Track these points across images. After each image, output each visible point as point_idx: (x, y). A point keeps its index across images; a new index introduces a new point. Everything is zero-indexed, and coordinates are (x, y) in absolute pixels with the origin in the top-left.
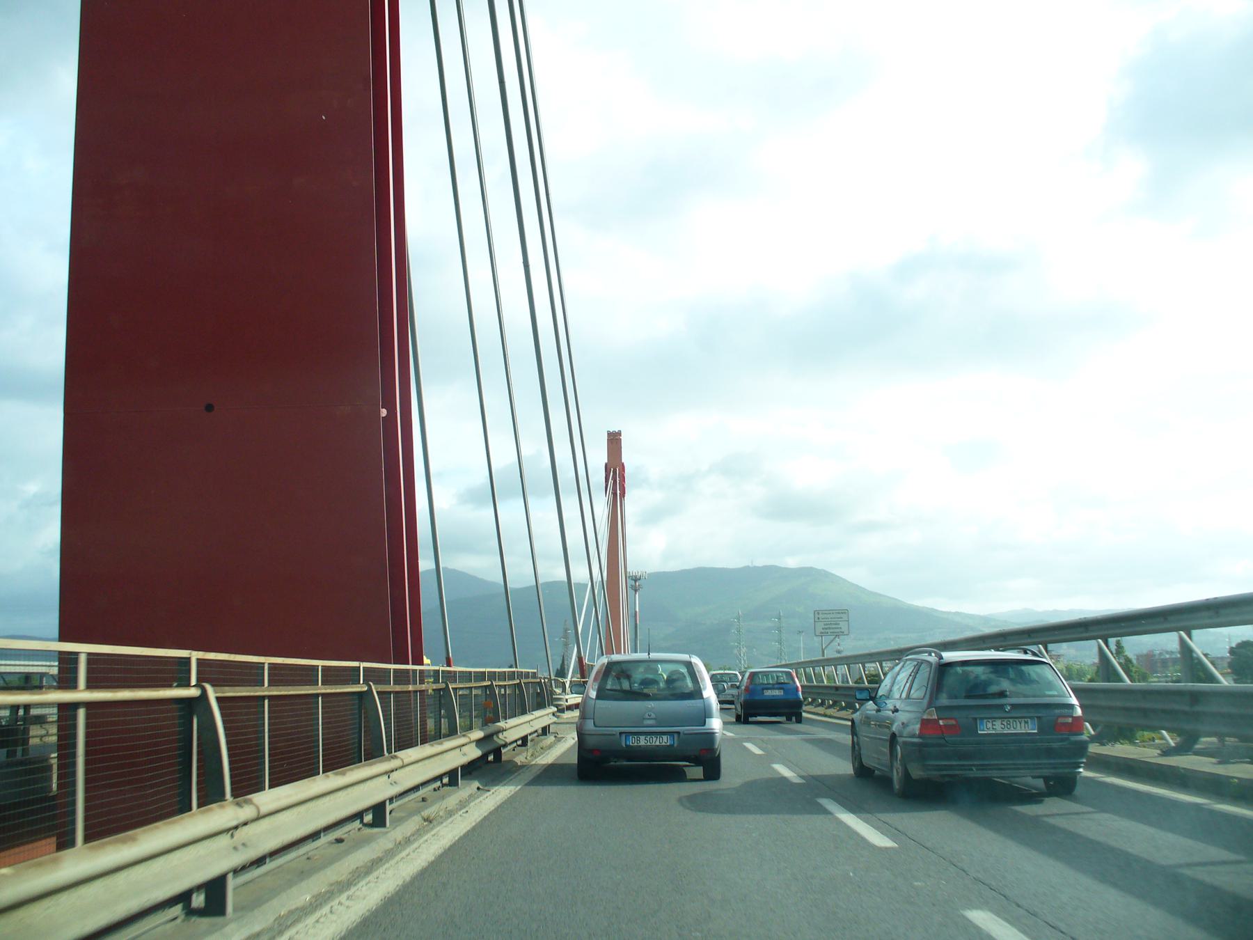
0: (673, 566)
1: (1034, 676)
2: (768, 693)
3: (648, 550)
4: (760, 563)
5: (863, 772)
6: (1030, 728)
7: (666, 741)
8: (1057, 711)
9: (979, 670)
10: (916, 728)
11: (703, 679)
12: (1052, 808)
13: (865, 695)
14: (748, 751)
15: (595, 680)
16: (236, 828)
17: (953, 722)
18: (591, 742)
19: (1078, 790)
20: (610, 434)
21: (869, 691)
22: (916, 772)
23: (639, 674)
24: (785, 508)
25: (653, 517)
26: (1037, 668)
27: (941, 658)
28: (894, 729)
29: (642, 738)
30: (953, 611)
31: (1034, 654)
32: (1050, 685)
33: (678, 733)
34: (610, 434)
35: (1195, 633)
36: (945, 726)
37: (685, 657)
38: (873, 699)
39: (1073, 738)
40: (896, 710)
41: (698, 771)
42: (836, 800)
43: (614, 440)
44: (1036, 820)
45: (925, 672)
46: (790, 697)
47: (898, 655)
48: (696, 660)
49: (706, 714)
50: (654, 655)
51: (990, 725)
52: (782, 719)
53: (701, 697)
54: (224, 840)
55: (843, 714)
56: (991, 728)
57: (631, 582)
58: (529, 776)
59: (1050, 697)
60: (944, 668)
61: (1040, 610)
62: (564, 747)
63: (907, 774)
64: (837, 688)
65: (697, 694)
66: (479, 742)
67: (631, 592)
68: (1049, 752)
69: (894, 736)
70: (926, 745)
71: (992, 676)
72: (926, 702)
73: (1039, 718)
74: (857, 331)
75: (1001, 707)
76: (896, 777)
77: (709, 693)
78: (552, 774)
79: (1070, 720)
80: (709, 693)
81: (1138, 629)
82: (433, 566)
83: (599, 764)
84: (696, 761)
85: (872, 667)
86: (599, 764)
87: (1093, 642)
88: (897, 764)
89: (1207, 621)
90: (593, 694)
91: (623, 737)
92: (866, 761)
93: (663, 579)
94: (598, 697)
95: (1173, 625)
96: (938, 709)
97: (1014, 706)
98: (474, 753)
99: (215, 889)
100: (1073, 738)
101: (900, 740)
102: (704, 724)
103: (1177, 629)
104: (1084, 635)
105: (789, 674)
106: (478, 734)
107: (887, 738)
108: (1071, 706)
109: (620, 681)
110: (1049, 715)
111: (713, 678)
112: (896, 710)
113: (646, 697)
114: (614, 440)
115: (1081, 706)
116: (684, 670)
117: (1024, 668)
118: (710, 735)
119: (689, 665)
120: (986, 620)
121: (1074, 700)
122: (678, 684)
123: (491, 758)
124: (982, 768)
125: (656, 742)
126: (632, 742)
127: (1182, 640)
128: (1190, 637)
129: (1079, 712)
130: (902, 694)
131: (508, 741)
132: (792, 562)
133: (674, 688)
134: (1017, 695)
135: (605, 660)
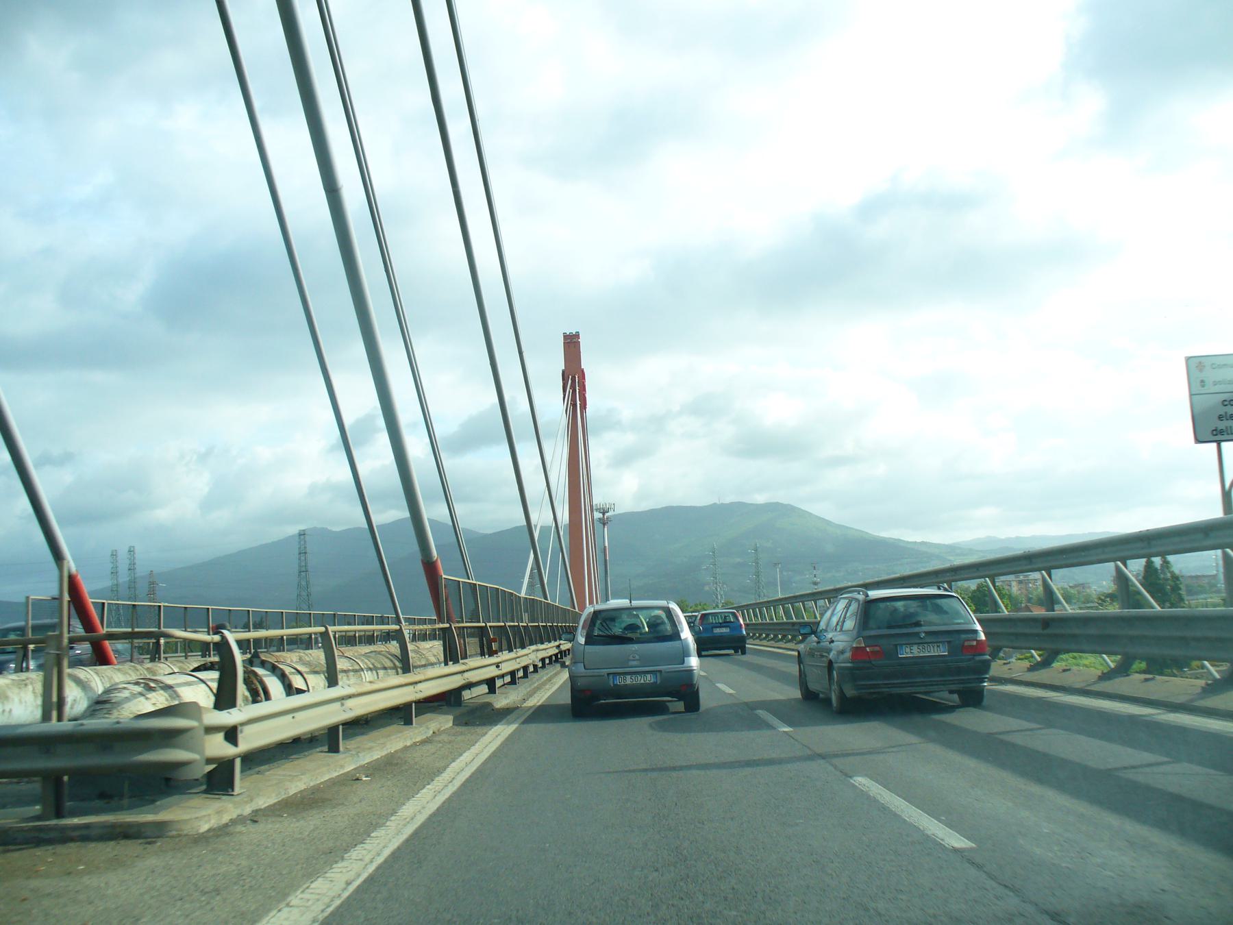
0: (644, 506)
2: (717, 631)
3: (619, 487)
4: (728, 499)
5: (809, 696)
6: (942, 651)
7: (649, 679)
8: (963, 636)
10: (848, 655)
11: (680, 623)
12: (969, 719)
13: (807, 630)
14: (719, 681)
17: (877, 649)
18: (580, 683)
19: (985, 702)
20: (566, 337)
22: (850, 692)
23: (627, 620)
24: (757, 445)
25: (624, 459)
28: (831, 656)
30: (919, 540)
31: (945, 590)
32: (957, 614)
34: (566, 337)
35: (1129, 562)
37: (663, 603)
38: (814, 632)
39: (978, 658)
40: (832, 641)
43: (572, 343)
45: (854, 607)
46: (736, 633)
47: (832, 595)
48: (673, 606)
49: (685, 653)
50: (636, 603)
53: (679, 638)
55: (789, 645)
56: (908, 652)
57: (597, 515)
60: (870, 603)
62: (554, 686)
65: (676, 636)
67: (598, 526)
68: (959, 671)
69: (830, 663)
70: (858, 669)
71: (919, 610)
72: (855, 632)
73: (949, 642)
74: (822, 271)
75: (917, 634)
77: (686, 634)
80: (686, 634)
82: (407, 514)
83: (590, 703)
86: (590, 703)
87: (1112, 564)
88: (835, 687)
90: (582, 640)
92: (813, 686)
93: (632, 519)
94: (586, 643)
97: (928, 633)
100: (978, 658)
101: (835, 665)
103: (1114, 560)
107: (826, 665)
108: (976, 632)
109: (608, 630)
110: (958, 638)
111: (248, 640)
112: (832, 641)
113: (629, 641)
114: (572, 343)
116: (663, 615)
117: (939, 601)
118: (690, 672)
119: (668, 612)
120: (952, 549)
121: (978, 627)
122: (661, 628)
124: (926, 693)
125: (641, 680)
126: (619, 681)
127: (1117, 568)
128: (1125, 565)
129: (982, 637)
130: (839, 625)
132: (760, 499)
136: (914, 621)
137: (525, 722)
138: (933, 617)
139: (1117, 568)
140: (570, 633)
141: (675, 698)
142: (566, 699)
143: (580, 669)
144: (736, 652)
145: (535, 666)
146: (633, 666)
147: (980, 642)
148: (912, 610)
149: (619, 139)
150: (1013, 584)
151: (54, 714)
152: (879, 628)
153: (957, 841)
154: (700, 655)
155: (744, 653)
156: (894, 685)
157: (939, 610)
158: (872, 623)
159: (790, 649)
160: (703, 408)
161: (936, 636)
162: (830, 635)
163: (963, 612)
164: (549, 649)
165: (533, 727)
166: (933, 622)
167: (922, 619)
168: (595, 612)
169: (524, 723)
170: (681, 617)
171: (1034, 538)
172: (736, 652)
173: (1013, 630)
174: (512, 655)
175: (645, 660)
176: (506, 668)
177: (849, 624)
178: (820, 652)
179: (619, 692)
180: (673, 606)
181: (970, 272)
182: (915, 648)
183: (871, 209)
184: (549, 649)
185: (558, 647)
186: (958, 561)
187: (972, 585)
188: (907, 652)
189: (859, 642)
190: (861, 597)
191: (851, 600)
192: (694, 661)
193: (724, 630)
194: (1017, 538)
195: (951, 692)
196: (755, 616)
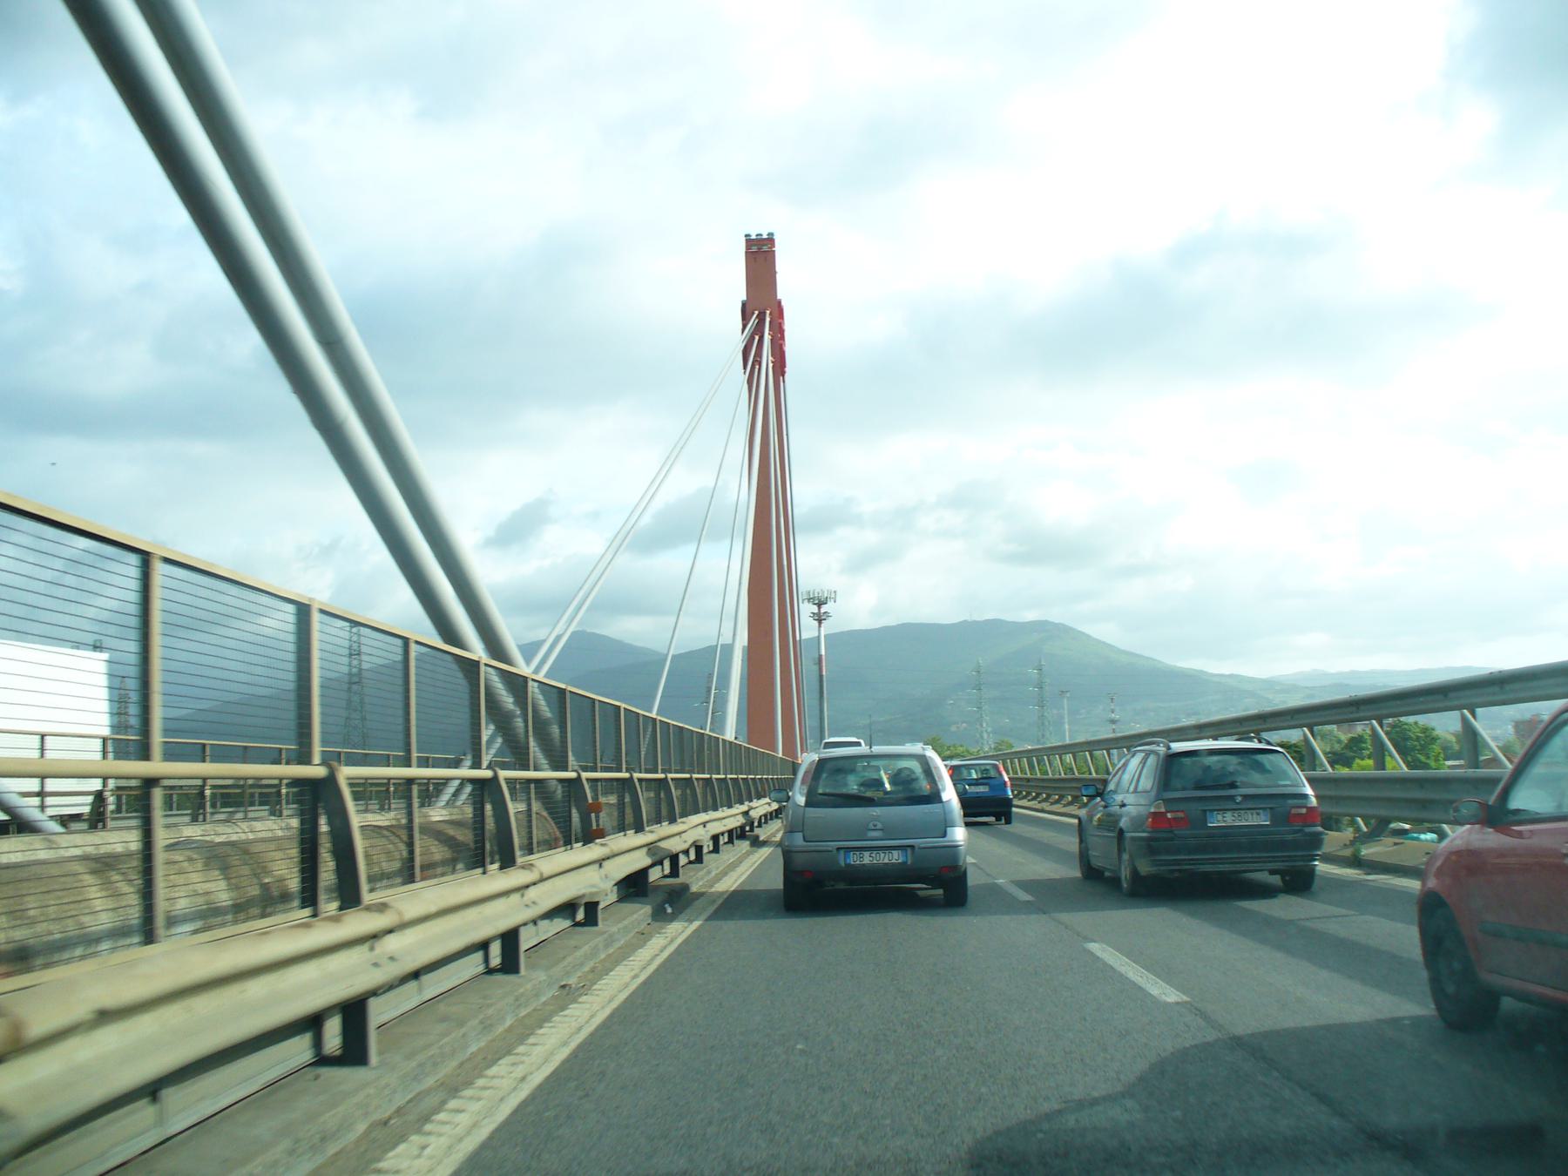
1: (1268, 766)
5: (1092, 873)
6: (1261, 820)
7: (896, 857)
9: (1233, 760)
11: (941, 777)
12: (1284, 907)
15: (803, 782)
16: (527, 887)
17: (1181, 815)
18: (800, 861)
19: (1316, 884)
20: (750, 242)
21: (1099, 789)
22: (1145, 868)
26: (1270, 757)
27: (1169, 748)
29: (866, 854)
32: (1284, 774)
33: (912, 847)
35: (1479, 711)
36: (1174, 819)
37: (916, 748)
38: (1100, 794)
39: (1307, 830)
40: (1123, 805)
43: (760, 253)
44: (1269, 922)
45: (1152, 760)
47: (1129, 742)
48: (931, 753)
49: (945, 825)
50: (877, 749)
52: (992, 819)
54: (515, 897)
56: (1221, 820)
59: (1284, 786)
63: (1135, 873)
64: (1028, 780)
65: (934, 797)
68: (1283, 845)
69: (1121, 832)
72: (1153, 793)
74: (1124, 327)
75: (1232, 798)
76: (1125, 873)
77: (949, 794)
78: (738, 904)
79: (1304, 811)
80: (949, 794)
81: (1522, 695)
84: (934, 880)
86: (813, 889)
87: (1456, 714)
89: (1491, 698)
95: (1456, 703)
96: (1167, 801)
97: (1246, 797)
100: (1307, 830)
101: (1128, 835)
102: (944, 835)
103: (1459, 708)
104: (1441, 705)
105: (996, 767)
108: (1305, 796)
109: (837, 785)
110: (1281, 803)
112: (1123, 805)
114: (760, 253)
115: (1317, 797)
117: (1260, 757)
119: (922, 759)
120: (1270, 684)
121: (1309, 791)
122: (915, 785)
125: (884, 858)
126: (854, 859)
128: (1474, 716)
129: (1314, 801)
130: (1133, 784)
133: (913, 790)
134: (1245, 785)
135: (816, 757)
136: (1229, 780)
137: (715, 916)
138: (1256, 777)
139: (1464, 719)
140: (782, 789)
141: (939, 886)
142: (775, 881)
143: (798, 840)
144: (998, 819)
145: (699, 849)
147: (1311, 809)
148: (1231, 768)
152: (1184, 789)
153: (1171, 996)
154: (967, 824)
155: (1008, 822)
156: (1222, 861)
157: (1260, 768)
158: (1176, 783)
159: (1068, 815)
161: (1256, 801)
162: (1119, 798)
163: (1291, 772)
164: (730, 818)
165: (729, 926)
166: (1256, 783)
167: (1239, 779)
169: (709, 919)
170: (941, 768)
171: (1373, 672)
172: (998, 819)
173: (1332, 793)
174: (515, 878)
175: (888, 832)
176: (690, 837)
177: (1146, 783)
178: (1110, 822)
179: (856, 875)
180: (931, 753)
182: (1229, 816)
184: (730, 818)
185: (746, 813)
187: (1294, 735)
188: (1218, 821)
189: (1158, 806)
190: (1161, 749)
191: (1148, 754)
192: (959, 834)
193: (981, 789)
194: (1353, 672)
195: (1272, 872)
196: (1032, 767)
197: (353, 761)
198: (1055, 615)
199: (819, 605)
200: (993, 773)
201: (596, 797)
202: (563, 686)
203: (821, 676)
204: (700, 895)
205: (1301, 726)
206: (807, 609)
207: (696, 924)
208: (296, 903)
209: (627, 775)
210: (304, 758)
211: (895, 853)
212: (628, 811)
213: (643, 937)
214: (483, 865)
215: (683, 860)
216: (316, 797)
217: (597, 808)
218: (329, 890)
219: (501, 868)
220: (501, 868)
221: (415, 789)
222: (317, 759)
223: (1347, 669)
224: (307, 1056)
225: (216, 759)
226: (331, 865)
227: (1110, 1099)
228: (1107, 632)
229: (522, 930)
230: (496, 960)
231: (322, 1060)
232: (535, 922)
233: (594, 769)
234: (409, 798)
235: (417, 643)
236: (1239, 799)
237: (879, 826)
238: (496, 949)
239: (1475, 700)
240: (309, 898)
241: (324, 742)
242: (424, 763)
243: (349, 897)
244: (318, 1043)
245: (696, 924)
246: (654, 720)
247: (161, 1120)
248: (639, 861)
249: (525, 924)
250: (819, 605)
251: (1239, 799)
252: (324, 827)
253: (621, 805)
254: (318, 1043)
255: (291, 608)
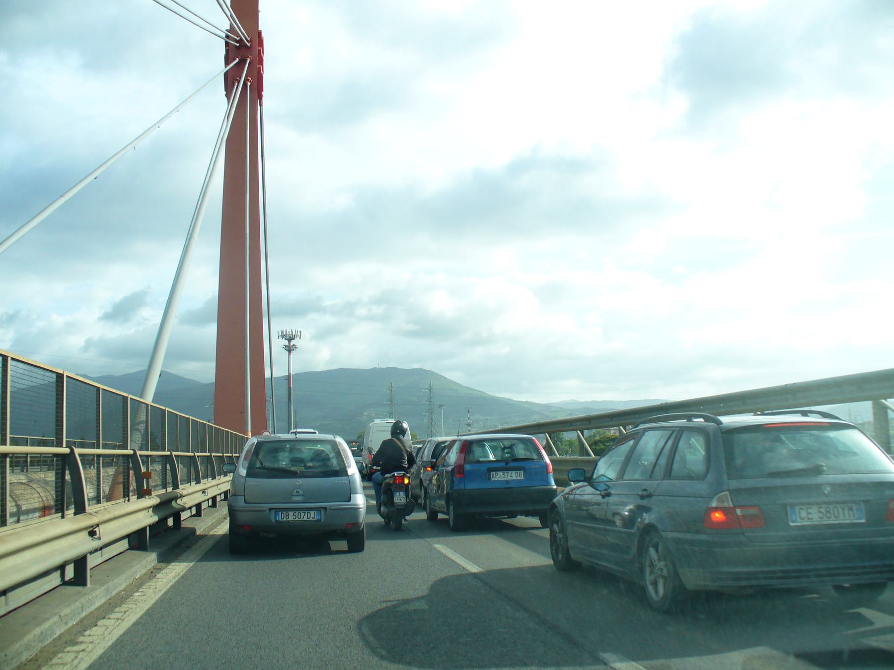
2: (499, 477)
7: (313, 516)
11: (347, 457)
15: (245, 459)
17: (752, 511)
18: (243, 518)
24: (427, 328)
29: (291, 513)
30: (524, 400)
33: (325, 508)
41: (343, 545)
42: (867, 606)
48: (340, 440)
51: (804, 514)
53: (346, 474)
58: (205, 546)
61: (582, 400)
62: (217, 525)
65: (342, 472)
66: (156, 508)
74: (482, 207)
75: (819, 487)
77: (353, 470)
80: (353, 470)
85: (513, 442)
86: (254, 539)
90: (243, 472)
91: (273, 512)
92: (574, 556)
94: (249, 475)
97: (835, 486)
98: (148, 519)
99: (80, 563)
106: (152, 500)
109: (267, 462)
118: (356, 509)
119: (334, 445)
120: (548, 407)
123: (170, 522)
125: (304, 517)
126: (281, 517)
131: (187, 506)
133: (328, 466)
146: (293, 502)
149: (346, 105)
150: (569, 436)
151: (120, 488)
160: (388, 300)
168: (259, 445)
171: (605, 402)
174: (215, 482)
175: (309, 496)
176: (211, 493)
181: (581, 214)
183: (518, 168)
186: (561, 417)
194: (593, 402)
197: (83, 445)
198: (428, 366)
199: (290, 340)
200: (521, 451)
201: (148, 468)
202: (126, 395)
203: (290, 388)
204: (202, 537)
205: (576, 430)
206: (279, 344)
207: (192, 564)
208: (54, 511)
209: (169, 453)
210: (60, 445)
211: (312, 513)
212: (169, 472)
213: (152, 574)
214: (62, 511)
215: (218, 499)
216: (65, 462)
217: (148, 475)
218: (134, 490)
219: (75, 514)
220: (75, 514)
221: (8, 460)
222: (64, 445)
223: (590, 400)
224: (58, 581)
225: (32, 445)
226: (134, 484)
227: (418, 599)
228: (456, 376)
229: (89, 556)
230: (210, 504)
231: (65, 583)
232: (101, 549)
233: (177, 451)
234: (98, 464)
235: (13, 359)
236: (827, 490)
237: (301, 492)
238: (210, 501)
239: (625, 422)
240: (126, 495)
241: (67, 437)
242: (105, 447)
243: (80, 509)
244: (63, 575)
245: (192, 564)
246: (147, 405)
247: (7, 603)
248: (81, 544)
249: (91, 553)
250: (290, 340)
251: (827, 490)
252: (68, 477)
253: (164, 470)
254: (63, 575)
255: (54, 376)
